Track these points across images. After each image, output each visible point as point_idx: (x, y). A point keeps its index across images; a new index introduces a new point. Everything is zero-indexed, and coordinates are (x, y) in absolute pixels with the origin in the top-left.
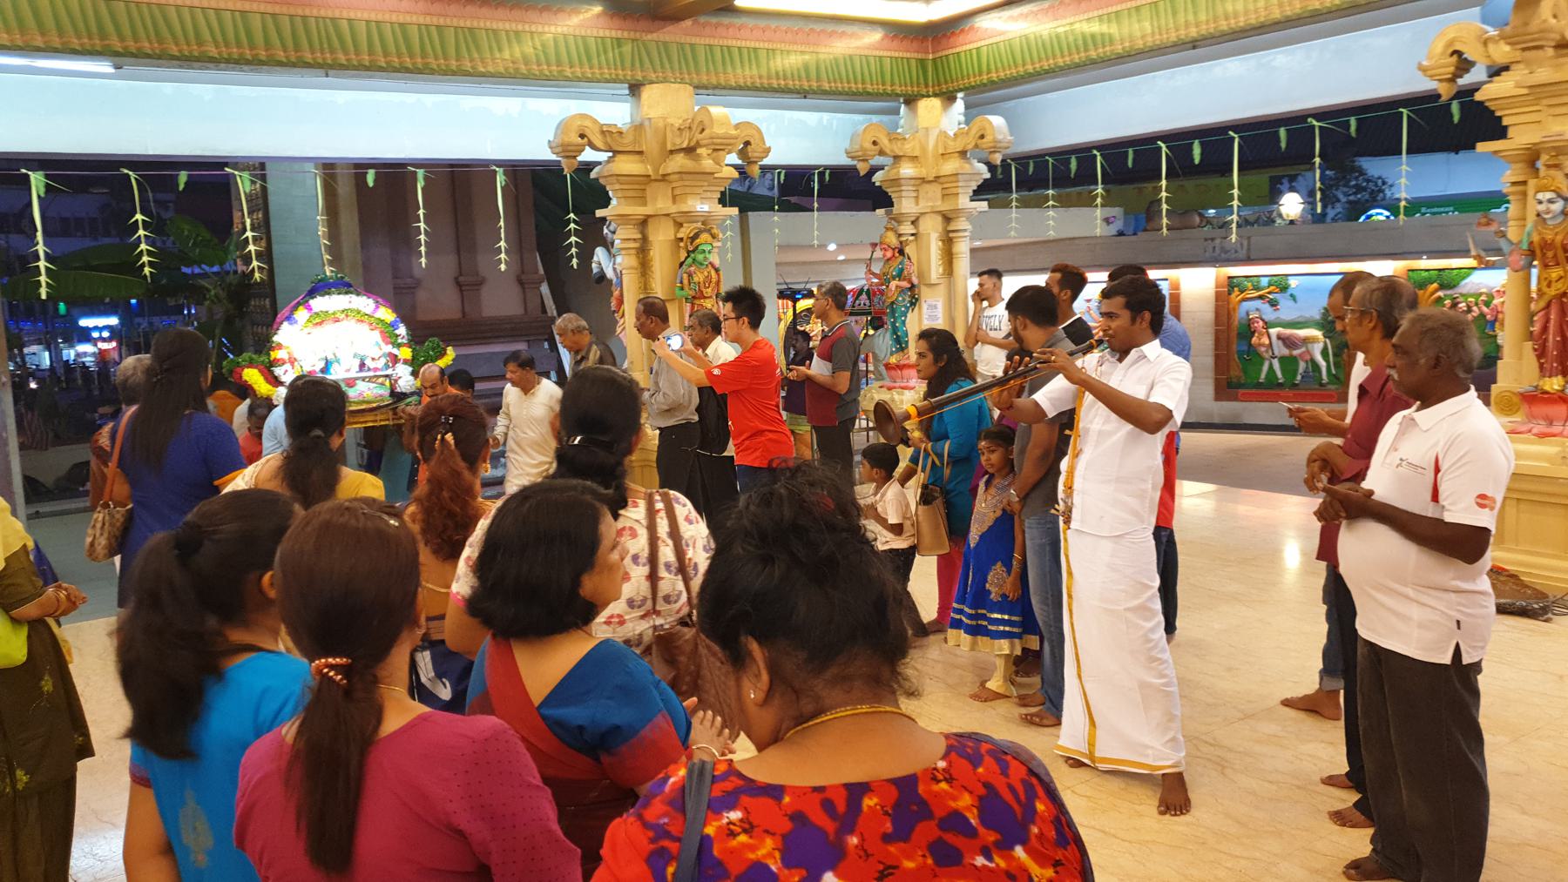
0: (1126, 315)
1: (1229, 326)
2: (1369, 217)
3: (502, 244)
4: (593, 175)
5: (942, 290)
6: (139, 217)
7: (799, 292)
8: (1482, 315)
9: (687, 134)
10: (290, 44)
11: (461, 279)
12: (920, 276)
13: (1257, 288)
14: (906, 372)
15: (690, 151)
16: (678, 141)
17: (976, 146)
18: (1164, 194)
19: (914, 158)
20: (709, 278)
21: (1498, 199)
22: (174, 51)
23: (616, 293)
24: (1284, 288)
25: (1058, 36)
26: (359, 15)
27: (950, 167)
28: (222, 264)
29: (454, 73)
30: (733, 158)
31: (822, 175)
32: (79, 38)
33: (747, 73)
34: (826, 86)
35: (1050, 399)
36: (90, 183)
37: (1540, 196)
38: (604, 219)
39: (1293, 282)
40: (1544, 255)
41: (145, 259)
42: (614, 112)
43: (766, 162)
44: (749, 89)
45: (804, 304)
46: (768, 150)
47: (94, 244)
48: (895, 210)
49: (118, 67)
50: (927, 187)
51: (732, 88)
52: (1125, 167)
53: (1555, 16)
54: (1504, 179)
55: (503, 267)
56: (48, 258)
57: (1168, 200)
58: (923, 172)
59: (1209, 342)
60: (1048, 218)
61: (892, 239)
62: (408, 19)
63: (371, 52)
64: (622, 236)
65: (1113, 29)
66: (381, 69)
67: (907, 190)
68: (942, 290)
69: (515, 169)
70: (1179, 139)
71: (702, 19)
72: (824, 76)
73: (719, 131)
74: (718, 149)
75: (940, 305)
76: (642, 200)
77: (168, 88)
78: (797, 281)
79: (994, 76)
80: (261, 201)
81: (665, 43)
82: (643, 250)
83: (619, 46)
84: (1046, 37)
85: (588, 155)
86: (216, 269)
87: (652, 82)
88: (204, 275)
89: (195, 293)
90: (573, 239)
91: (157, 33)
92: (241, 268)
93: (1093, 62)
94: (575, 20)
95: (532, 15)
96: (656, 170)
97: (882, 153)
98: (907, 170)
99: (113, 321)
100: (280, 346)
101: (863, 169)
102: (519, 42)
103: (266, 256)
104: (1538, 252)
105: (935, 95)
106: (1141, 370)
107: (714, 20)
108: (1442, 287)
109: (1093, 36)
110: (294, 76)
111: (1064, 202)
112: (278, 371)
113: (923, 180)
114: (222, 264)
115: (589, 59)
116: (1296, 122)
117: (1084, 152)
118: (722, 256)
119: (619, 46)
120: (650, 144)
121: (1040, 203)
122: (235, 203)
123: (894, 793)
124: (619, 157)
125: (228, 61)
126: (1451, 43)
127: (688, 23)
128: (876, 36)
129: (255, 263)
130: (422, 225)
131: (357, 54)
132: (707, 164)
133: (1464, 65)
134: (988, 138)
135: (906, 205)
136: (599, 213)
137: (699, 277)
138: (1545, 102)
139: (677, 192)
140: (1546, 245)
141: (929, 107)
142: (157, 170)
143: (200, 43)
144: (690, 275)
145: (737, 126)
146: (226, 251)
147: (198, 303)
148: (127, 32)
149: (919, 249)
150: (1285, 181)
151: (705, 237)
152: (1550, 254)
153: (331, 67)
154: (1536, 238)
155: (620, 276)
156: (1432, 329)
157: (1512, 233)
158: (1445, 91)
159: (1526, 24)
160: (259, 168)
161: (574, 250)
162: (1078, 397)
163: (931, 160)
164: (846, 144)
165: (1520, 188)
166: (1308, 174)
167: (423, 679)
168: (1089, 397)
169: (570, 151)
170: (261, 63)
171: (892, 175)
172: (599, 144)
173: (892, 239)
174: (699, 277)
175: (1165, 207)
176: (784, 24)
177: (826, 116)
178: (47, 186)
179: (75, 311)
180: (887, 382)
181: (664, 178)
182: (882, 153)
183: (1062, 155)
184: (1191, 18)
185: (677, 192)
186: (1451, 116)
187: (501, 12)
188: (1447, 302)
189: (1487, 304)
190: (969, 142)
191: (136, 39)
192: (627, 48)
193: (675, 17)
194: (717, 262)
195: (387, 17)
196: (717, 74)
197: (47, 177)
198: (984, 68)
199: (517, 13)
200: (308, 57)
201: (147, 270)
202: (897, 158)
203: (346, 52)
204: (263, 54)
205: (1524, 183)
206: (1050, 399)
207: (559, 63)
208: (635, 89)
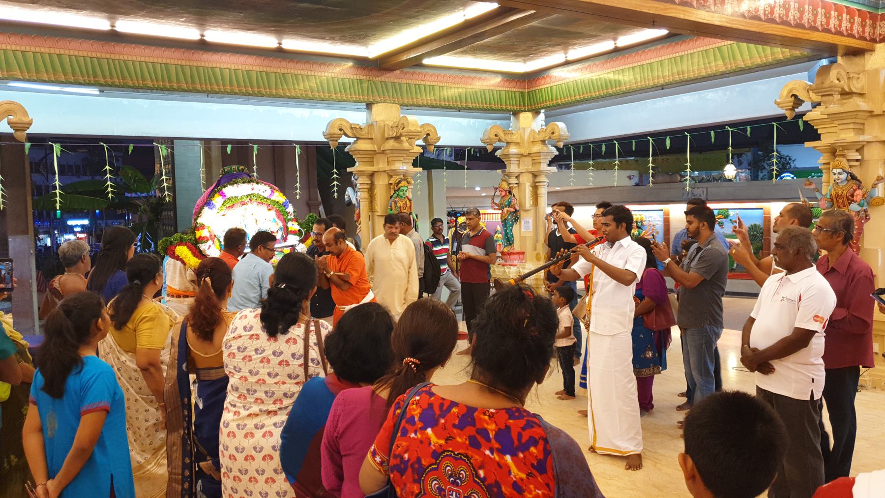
2: (781, 178)
3: (298, 185)
4: (346, 150)
5: (532, 213)
6: (107, 167)
9: (395, 130)
10: (189, 79)
12: (520, 206)
14: (512, 257)
15: (397, 138)
16: (391, 133)
18: (651, 165)
21: (817, 171)
23: (357, 212)
24: (726, 216)
26: (226, 66)
27: (536, 148)
28: (148, 192)
29: (274, 96)
30: (421, 142)
31: (469, 151)
33: (429, 98)
34: (470, 106)
35: (581, 268)
36: (86, 151)
37: (834, 171)
38: (351, 173)
39: (731, 213)
40: (837, 201)
41: (110, 189)
42: (358, 117)
43: (437, 144)
44: (429, 106)
45: (461, 220)
46: (439, 138)
47: (78, 180)
48: (507, 171)
49: (101, 91)
51: (420, 106)
52: (631, 149)
53: (838, 79)
54: (820, 161)
55: (298, 197)
56: (61, 188)
57: (653, 169)
58: (522, 151)
61: (505, 186)
62: (251, 68)
63: (231, 84)
64: (361, 182)
65: (621, 77)
66: (236, 94)
67: (514, 160)
68: (532, 213)
69: (307, 146)
70: (659, 136)
71: (406, 70)
73: (412, 128)
74: (412, 137)
75: (531, 221)
76: (372, 163)
77: (126, 101)
78: (458, 206)
80: (171, 159)
81: (385, 82)
82: (371, 189)
83: (361, 83)
84: (586, 82)
85: (344, 139)
86: (145, 194)
87: (378, 103)
88: (138, 198)
89: (132, 206)
90: (335, 183)
91: (122, 72)
92: (158, 194)
93: (611, 95)
94: (338, 69)
95: (315, 67)
96: (379, 148)
97: (500, 140)
98: (513, 150)
99: (86, 222)
100: (203, 227)
101: (490, 149)
102: (308, 80)
103: (173, 189)
105: (529, 111)
106: (621, 252)
107: (411, 70)
109: (610, 82)
110: (167, 95)
111: (597, 167)
112: (203, 247)
113: (522, 155)
114: (148, 192)
115: (345, 90)
116: (719, 128)
118: (414, 192)
119: (361, 83)
120: (376, 134)
121: (585, 168)
122: (156, 160)
123: (465, 411)
124: (360, 141)
125: (157, 89)
126: (791, 91)
127: (398, 72)
128: (498, 79)
129: (166, 193)
132: (406, 145)
133: (798, 101)
134: (556, 134)
135: (513, 168)
136: (349, 170)
137: (400, 204)
138: (836, 122)
139: (390, 159)
142: (118, 143)
144: (395, 203)
145: (422, 126)
146: (150, 185)
147: (134, 213)
148: (107, 73)
151: (404, 183)
152: (841, 201)
153: (210, 92)
154: (833, 193)
155: (359, 203)
156: (795, 236)
157: (825, 190)
158: (789, 115)
160: (170, 142)
161: (335, 189)
162: (593, 267)
164: (481, 136)
168: (596, 267)
169: (332, 137)
170: (174, 90)
171: (505, 152)
172: (349, 134)
173: (505, 186)
174: (400, 204)
175: (651, 171)
176: (448, 73)
177: (472, 120)
178: (61, 151)
179: (65, 216)
180: (502, 262)
181: (383, 152)
182: (500, 140)
183: (598, 143)
184: (660, 73)
185: (390, 159)
187: (299, 65)
192: (365, 85)
194: (410, 196)
195: (240, 67)
196: (412, 99)
199: (307, 66)
200: (199, 87)
201: (110, 195)
202: (508, 143)
203: (218, 85)
204: (175, 86)
205: (829, 164)
206: (581, 268)
208: (369, 106)
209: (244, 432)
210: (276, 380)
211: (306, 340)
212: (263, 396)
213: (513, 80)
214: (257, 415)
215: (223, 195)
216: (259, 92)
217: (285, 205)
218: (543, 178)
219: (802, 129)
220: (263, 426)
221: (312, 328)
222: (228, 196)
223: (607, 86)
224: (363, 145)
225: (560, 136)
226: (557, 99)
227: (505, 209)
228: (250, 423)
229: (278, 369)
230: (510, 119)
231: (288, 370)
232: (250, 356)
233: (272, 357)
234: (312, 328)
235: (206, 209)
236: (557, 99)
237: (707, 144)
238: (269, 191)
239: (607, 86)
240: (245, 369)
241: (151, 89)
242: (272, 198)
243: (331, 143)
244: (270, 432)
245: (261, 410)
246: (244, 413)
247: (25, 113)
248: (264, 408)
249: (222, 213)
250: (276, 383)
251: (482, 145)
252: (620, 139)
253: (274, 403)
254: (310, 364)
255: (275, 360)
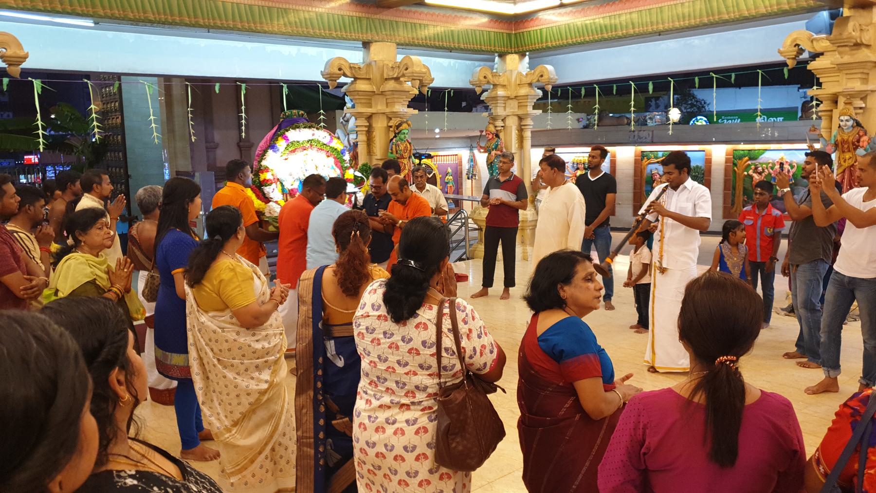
0: (676, 172)
1: (641, 177)
7: (423, 155)
8: (770, 174)
9: (397, 70)
11: (241, 144)
13: (656, 158)
15: (397, 79)
16: (391, 74)
17: (538, 81)
19: (504, 86)
20: (406, 147)
22: (131, 16)
25: (586, 25)
27: (524, 91)
31: (449, 93)
32: (81, 6)
34: (462, 46)
37: (842, 118)
40: (843, 147)
42: (355, 56)
43: (431, 85)
46: (433, 80)
49: (96, 23)
50: (510, 101)
59: (631, 185)
60: (568, 119)
61: (492, 128)
66: (239, 30)
67: (500, 102)
70: (641, 81)
71: (401, 8)
72: (461, 41)
77: (110, 34)
79: (550, 44)
81: (383, 20)
84: (580, 26)
85: (343, 80)
93: (606, 40)
96: (378, 89)
97: (488, 83)
98: (501, 92)
100: (267, 169)
101: (478, 90)
104: (840, 146)
105: (516, 53)
107: (407, 9)
108: (750, 159)
110: (192, 31)
112: (267, 189)
113: (509, 98)
117: (589, 86)
119: (360, 21)
120: (375, 74)
124: (358, 82)
125: (159, 23)
126: (795, 40)
130: (243, 115)
131: (227, 21)
133: (801, 51)
137: (402, 147)
140: (844, 142)
141: (512, 59)
143: (145, 12)
149: (505, 135)
150: (653, 100)
151: (405, 125)
152: (846, 146)
153: (213, 28)
154: (839, 138)
159: (841, 34)
163: (513, 87)
164: (470, 78)
165: (829, 113)
166: (666, 97)
167: (329, 355)
169: (332, 77)
170: (176, 24)
171: (493, 94)
172: (348, 74)
173: (492, 128)
177: (452, 61)
178: (42, 87)
181: (382, 93)
183: (577, 86)
186: (784, 75)
188: (753, 167)
189: (772, 168)
190: (534, 79)
191: (111, 8)
192: (364, 22)
193: (389, 7)
197: (42, 82)
198: (544, 40)
200: (201, 22)
202: (495, 85)
204: (177, 19)
207: (330, 30)
208: (366, 45)
209: (375, 425)
210: (407, 369)
211: (439, 325)
212: (393, 386)
213: (501, 22)
214: (389, 407)
215: (286, 138)
216: (197, 22)
217: (343, 152)
218: (529, 122)
219: (786, 77)
220: (394, 422)
221: (446, 311)
222: (291, 140)
223: (601, 30)
224: (362, 86)
225: (550, 79)
226: (547, 41)
227: (493, 153)
228: (382, 416)
229: (408, 358)
230: (494, 61)
231: (419, 359)
232: (378, 339)
233: (400, 343)
234: (446, 311)
235: (270, 152)
236: (547, 41)
237: (654, 90)
238: (328, 138)
239: (601, 30)
240: (375, 352)
241: (152, 22)
242: (332, 145)
243: (329, 83)
244: (401, 429)
245: (392, 402)
246: (375, 403)
247: (20, 46)
248: (396, 400)
249: (285, 157)
250: (407, 374)
251: (471, 87)
252: (600, 83)
253: (406, 395)
254: (444, 354)
255: (404, 347)
